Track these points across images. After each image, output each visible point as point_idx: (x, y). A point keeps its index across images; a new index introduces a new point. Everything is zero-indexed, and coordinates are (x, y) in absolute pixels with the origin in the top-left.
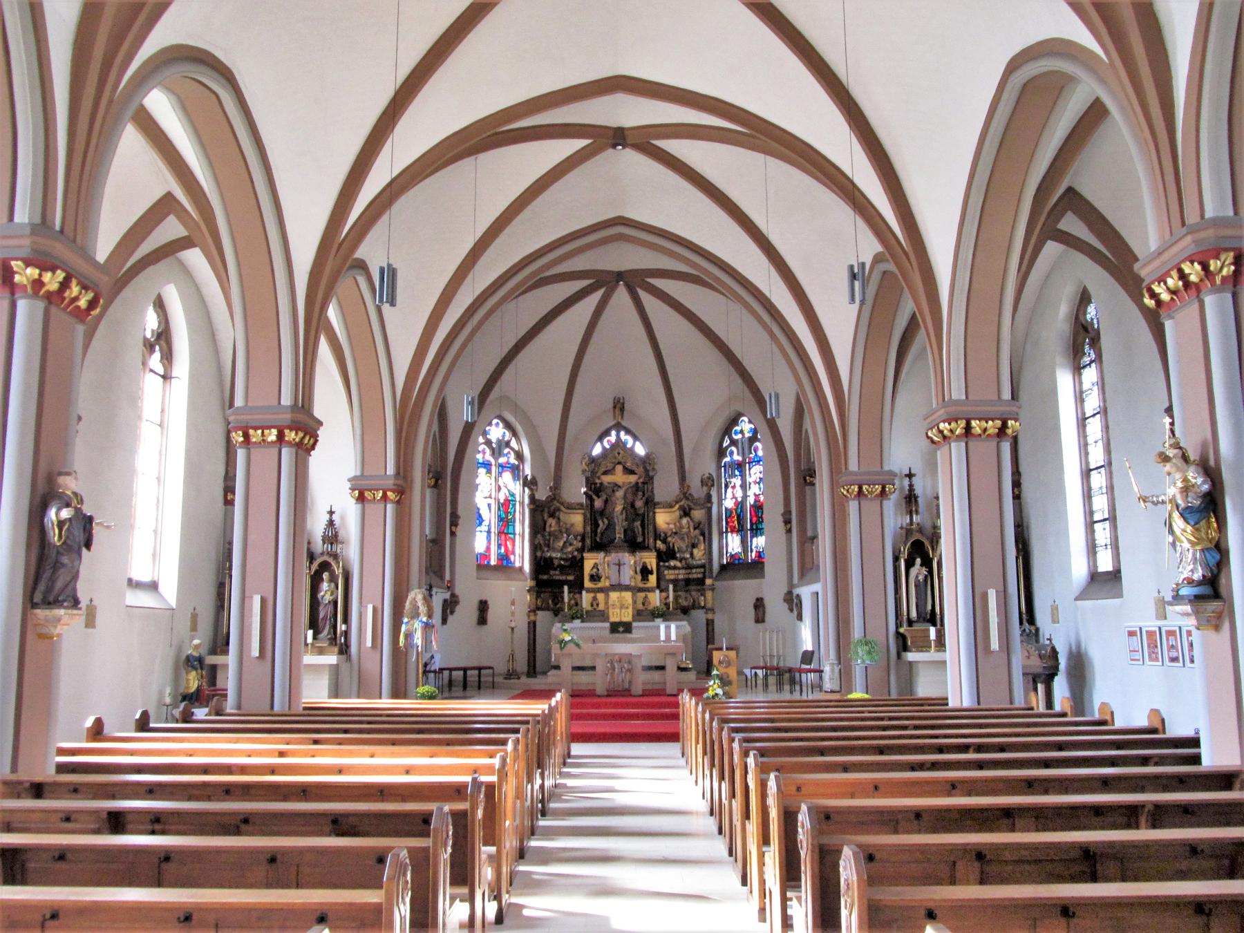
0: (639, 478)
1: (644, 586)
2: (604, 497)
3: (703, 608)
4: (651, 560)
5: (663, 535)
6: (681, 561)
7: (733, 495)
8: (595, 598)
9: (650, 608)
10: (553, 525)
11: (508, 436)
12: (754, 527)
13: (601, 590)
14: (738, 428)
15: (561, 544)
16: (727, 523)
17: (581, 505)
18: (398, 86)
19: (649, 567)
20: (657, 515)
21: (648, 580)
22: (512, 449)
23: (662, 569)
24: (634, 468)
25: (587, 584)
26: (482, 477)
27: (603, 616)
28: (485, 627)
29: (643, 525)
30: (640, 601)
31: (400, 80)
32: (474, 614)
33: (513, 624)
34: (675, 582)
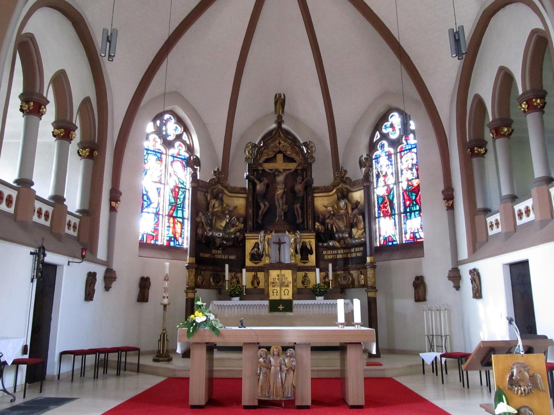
0: (298, 166)
1: (303, 265)
2: (266, 181)
3: (363, 286)
4: (311, 242)
5: (321, 217)
6: (339, 242)
7: (385, 182)
8: (255, 277)
9: (311, 286)
10: (216, 205)
11: (180, 130)
12: (408, 210)
13: (261, 269)
14: (388, 124)
15: (223, 224)
16: (379, 208)
17: (244, 189)
18: (170, 34)
19: (309, 247)
20: (316, 199)
21: (308, 259)
22: (184, 142)
23: (321, 250)
24: (293, 156)
25: (248, 263)
26: (151, 162)
27: (262, 294)
28: (145, 304)
29: (302, 208)
30: (299, 281)
31: (171, 32)
32: (135, 291)
33: (166, 301)
34: (334, 261)
